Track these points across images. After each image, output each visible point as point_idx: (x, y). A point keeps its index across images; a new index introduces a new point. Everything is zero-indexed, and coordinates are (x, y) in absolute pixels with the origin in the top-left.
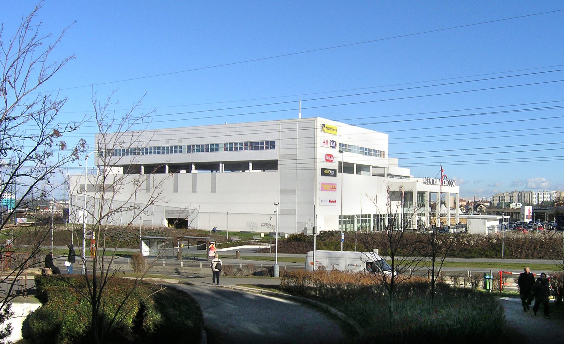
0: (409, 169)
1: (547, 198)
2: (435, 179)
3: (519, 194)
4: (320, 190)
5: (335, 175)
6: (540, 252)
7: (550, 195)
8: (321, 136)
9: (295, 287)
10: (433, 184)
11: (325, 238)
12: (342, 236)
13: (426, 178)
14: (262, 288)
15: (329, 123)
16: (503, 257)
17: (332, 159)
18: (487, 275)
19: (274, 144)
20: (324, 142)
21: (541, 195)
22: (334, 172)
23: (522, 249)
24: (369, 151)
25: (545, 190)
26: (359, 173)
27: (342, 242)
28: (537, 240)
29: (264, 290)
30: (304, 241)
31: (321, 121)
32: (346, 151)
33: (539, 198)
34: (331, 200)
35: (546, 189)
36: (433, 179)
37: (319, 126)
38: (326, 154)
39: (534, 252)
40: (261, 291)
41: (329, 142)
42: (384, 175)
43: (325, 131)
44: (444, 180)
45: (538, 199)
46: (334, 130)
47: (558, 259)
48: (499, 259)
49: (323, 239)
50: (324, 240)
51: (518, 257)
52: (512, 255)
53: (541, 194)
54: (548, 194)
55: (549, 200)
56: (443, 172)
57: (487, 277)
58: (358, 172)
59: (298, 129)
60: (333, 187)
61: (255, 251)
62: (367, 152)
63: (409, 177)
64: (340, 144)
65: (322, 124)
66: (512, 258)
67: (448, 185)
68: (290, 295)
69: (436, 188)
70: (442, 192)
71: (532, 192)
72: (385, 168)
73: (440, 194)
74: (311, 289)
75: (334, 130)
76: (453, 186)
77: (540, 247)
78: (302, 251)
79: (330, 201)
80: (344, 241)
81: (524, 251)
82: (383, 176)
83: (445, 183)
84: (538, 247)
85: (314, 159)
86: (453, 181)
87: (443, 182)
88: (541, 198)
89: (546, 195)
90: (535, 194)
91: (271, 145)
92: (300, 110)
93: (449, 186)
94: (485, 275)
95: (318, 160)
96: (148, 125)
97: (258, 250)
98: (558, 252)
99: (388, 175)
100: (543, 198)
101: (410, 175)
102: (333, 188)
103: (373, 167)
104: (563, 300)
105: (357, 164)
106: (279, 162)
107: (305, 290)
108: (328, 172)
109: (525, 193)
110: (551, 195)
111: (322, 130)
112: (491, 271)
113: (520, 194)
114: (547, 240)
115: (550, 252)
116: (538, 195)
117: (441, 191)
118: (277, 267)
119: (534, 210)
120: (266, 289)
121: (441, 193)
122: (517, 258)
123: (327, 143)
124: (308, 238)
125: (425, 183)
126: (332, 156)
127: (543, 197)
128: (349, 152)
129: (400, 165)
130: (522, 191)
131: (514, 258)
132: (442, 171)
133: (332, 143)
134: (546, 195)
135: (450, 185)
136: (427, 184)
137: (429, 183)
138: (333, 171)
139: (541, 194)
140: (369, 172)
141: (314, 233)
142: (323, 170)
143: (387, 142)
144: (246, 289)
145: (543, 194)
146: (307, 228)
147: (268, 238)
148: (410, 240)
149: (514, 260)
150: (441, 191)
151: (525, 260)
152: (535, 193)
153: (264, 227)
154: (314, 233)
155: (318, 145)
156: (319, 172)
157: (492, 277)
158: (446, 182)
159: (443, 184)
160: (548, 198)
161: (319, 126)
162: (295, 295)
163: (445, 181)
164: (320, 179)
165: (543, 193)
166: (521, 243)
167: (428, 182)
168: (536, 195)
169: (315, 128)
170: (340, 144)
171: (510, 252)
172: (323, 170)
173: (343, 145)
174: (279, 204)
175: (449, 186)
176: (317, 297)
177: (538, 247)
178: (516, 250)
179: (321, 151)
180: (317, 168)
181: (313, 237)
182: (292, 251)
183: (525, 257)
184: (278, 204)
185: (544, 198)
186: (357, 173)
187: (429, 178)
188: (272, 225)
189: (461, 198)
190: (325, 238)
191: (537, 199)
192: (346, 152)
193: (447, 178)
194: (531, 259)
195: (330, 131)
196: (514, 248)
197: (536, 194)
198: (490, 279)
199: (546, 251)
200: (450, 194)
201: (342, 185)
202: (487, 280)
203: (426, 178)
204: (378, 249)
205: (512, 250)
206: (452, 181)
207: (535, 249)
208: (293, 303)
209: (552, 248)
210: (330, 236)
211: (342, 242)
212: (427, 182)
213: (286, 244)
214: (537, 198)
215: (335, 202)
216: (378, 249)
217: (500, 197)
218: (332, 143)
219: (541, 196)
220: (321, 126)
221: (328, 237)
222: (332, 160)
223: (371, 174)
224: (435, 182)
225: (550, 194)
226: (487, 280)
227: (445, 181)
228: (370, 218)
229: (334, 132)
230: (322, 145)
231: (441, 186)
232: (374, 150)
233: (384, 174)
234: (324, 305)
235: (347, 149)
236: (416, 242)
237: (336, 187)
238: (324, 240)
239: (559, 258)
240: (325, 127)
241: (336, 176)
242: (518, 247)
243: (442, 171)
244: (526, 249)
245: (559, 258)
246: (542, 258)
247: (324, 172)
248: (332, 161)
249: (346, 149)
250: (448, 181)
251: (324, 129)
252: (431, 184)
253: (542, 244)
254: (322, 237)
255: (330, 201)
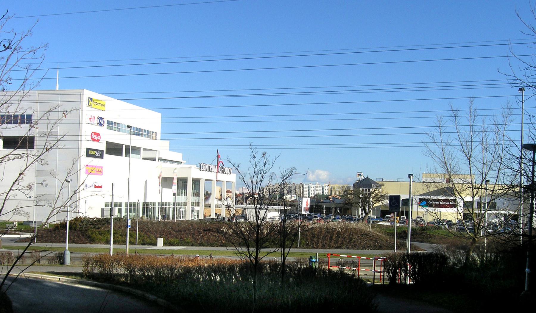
0: (181, 154)
1: (318, 191)
2: (211, 165)
3: (290, 187)
4: (85, 173)
5: (101, 157)
6: (337, 241)
7: (322, 189)
8: (88, 112)
9: (101, 274)
10: (209, 170)
11: (100, 226)
12: (129, 222)
13: (202, 164)
14: (59, 275)
15: (96, 96)
16: (299, 247)
17: (98, 138)
18: (313, 258)
19: (31, 118)
20: (90, 119)
21: (313, 188)
22: (101, 153)
23: (318, 238)
24: (139, 131)
25: (317, 183)
26: (128, 155)
27: (128, 229)
28: (333, 230)
29: (63, 278)
30: (75, 230)
31: (87, 94)
32: (114, 130)
33: (311, 191)
34: (97, 185)
35: (318, 182)
36: (209, 165)
37: (85, 98)
38: (93, 132)
39: (331, 242)
40: (60, 279)
41: (96, 118)
42: (155, 159)
43: (92, 106)
44: (220, 167)
45: (310, 192)
46: (102, 105)
47: (356, 249)
48: (295, 249)
49: (97, 227)
50: (99, 228)
51: (315, 247)
52: (308, 244)
53: (313, 187)
54: (320, 187)
55: (321, 193)
56: (219, 158)
57: (314, 260)
58: (127, 153)
59: (60, 101)
60: (100, 171)
61: (16, 241)
62: (138, 132)
63: (181, 162)
64: (108, 122)
65: (89, 98)
66: (309, 248)
67: (225, 173)
68: (96, 283)
69: (212, 176)
70: (218, 180)
71: (303, 185)
72: (156, 151)
73: (216, 182)
74: (121, 275)
75: (102, 105)
76: (229, 173)
77: (336, 237)
78: (73, 241)
79: (96, 187)
80: (130, 227)
81: (320, 241)
82: (154, 160)
83: (221, 171)
84: (334, 237)
85: (78, 135)
86: (229, 168)
87: (220, 168)
88: (312, 191)
89: (318, 189)
90: (306, 187)
91: (26, 119)
92: (58, 79)
93: (225, 173)
94: (311, 258)
95: (83, 138)
96: (43, 77)
97: (18, 239)
98: (355, 242)
99: (159, 159)
100: (315, 191)
101: (183, 160)
102: (100, 171)
103: (144, 149)
104: (416, 275)
105: (126, 145)
106: (36, 139)
107: (113, 277)
108: (94, 153)
109: (296, 185)
110: (323, 188)
111: (89, 105)
112: (317, 254)
113: (291, 186)
114: (343, 229)
115: (347, 242)
116: (310, 188)
117: (217, 179)
118: (68, 254)
119: (311, 202)
120: (65, 276)
121: (217, 181)
122: (313, 247)
123: (94, 119)
124: (80, 226)
125: (201, 169)
126: (99, 135)
127: (314, 190)
128: (117, 131)
129: (172, 148)
130: (292, 183)
131: (311, 248)
132: (218, 156)
133: (100, 120)
134: (318, 189)
135: (227, 173)
136: (203, 171)
137: (204, 170)
138: (100, 152)
139: (313, 187)
140: (129, 158)
141: (111, 215)
142: (88, 150)
143: (160, 120)
144: (40, 276)
145: (315, 186)
146: (104, 210)
147: (24, 227)
148: (198, 228)
149: (311, 250)
150: (217, 179)
151: (322, 250)
152: (306, 185)
153: (16, 215)
154: (111, 215)
155: (84, 121)
156: (84, 152)
157: (317, 260)
158: (222, 170)
159: (219, 171)
160: (320, 191)
161: (85, 98)
162: (100, 282)
163: (221, 168)
164: (85, 161)
165: (314, 186)
166: (316, 233)
167: (204, 168)
168: (308, 188)
169: (81, 101)
170: (108, 122)
171: (305, 242)
172: (88, 150)
173: (112, 123)
174: (71, 180)
175: (225, 173)
176: (128, 283)
177: (334, 237)
178: (312, 240)
179: (87, 129)
180: (82, 148)
181: (111, 219)
182: (61, 240)
183: (322, 246)
184: (70, 181)
185: (316, 191)
186: (126, 156)
187: (204, 164)
188: (26, 212)
189: (228, 189)
190: (100, 226)
191: (308, 192)
192: (114, 131)
193: (223, 164)
194: (328, 248)
195: (97, 107)
196: (310, 237)
197: (308, 187)
198: (316, 262)
199: (342, 241)
200: (226, 182)
201: (129, 165)
202: (313, 263)
203: (202, 164)
204: (163, 238)
205: (307, 239)
206: (228, 168)
207: (331, 238)
208: (104, 290)
209: (348, 238)
210: (105, 224)
211: (128, 229)
212: (203, 168)
213: (53, 232)
214: (308, 191)
215: (101, 187)
216: (163, 238)
217: (270, 189)
218: (100, 120)
219: (312, 189)
220: (88, 99)
221: (103, 224)
222: (99, 139)
223: (141, 158)
224: (211, 168)
225: (322, 187)
226: (313, 263)
227: (221, 168)
228: (125, 208)
229: (102, 108)
230: (88, 121)
231: (217, 173)
232: (145, 130)
233: (155, 158)
234: (140, 292)
235: (116, 128)
236: (204, 231)
237: (103, 170)
238: (99, 228)
239: (356, 248)
240: (92, 101)
241: (103, 158)
242: (314, 237)
243: (218, 156)
244: (322, 238)
245: (356, 248)
246: (339, 248)
247: (90, 153)
248: (98, 141)
249: (114, 127)
250: (225, 168)
251: (90, 102)
252: (207, 170)
253: (339, 233)
254: (96, 225)
255: (96, 187)
